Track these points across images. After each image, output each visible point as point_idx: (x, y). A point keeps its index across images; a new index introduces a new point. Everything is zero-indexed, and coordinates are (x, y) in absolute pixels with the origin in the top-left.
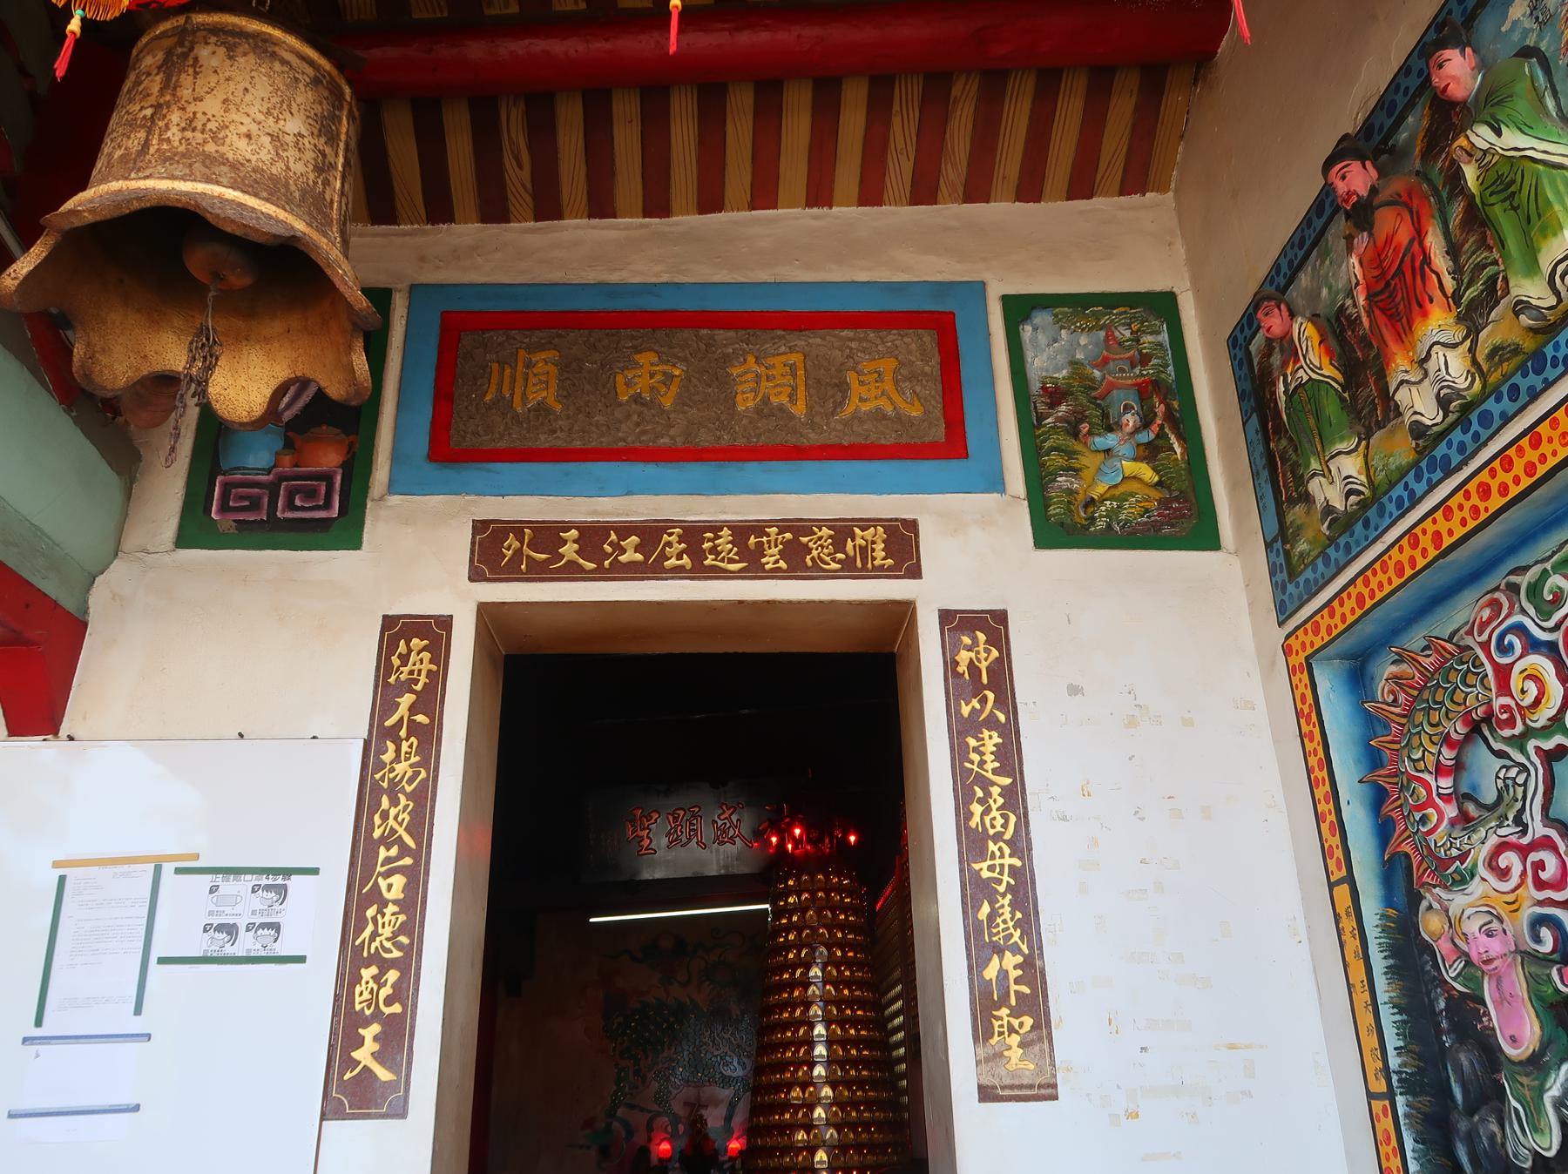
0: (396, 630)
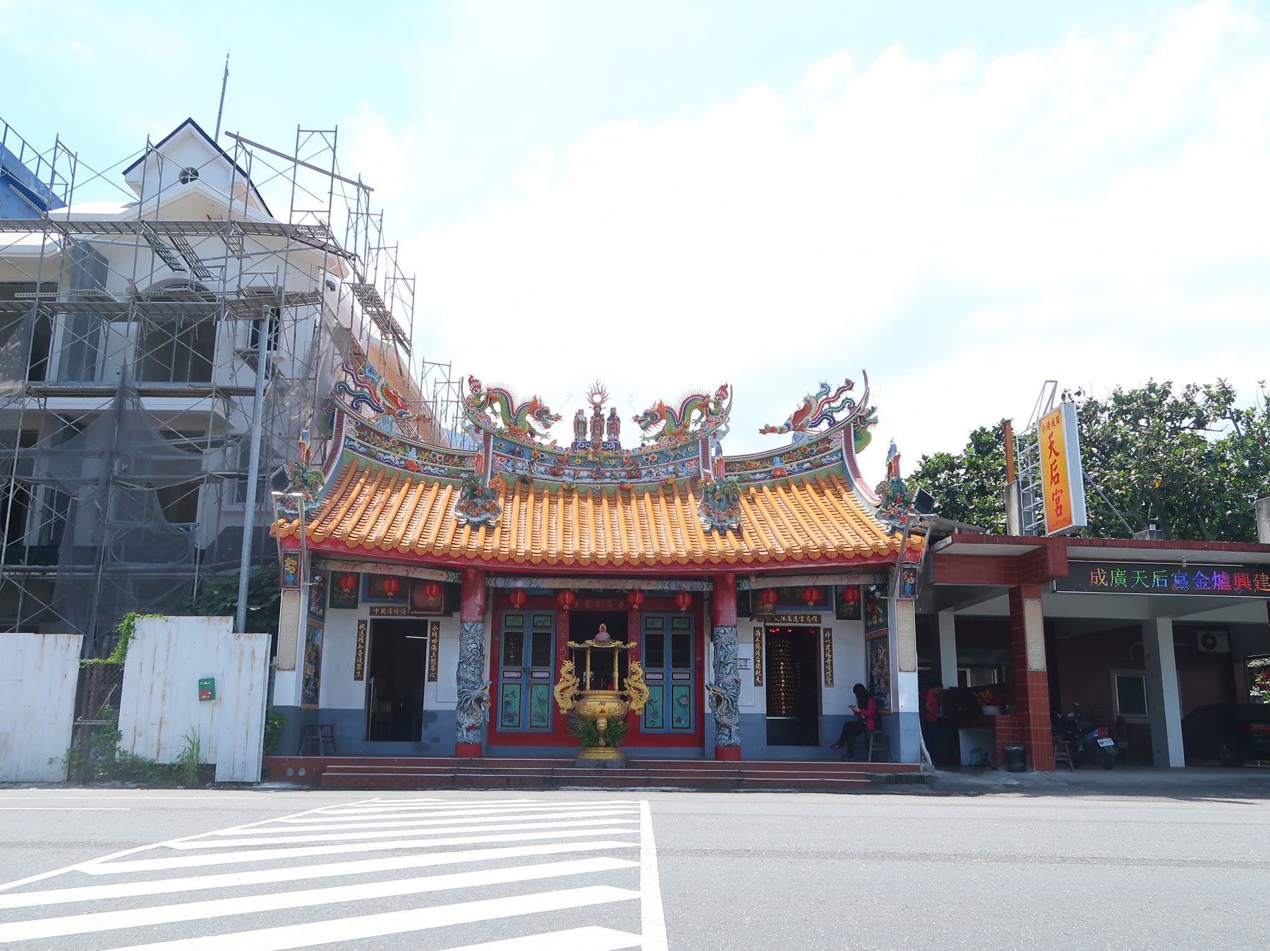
0: (360, 622)
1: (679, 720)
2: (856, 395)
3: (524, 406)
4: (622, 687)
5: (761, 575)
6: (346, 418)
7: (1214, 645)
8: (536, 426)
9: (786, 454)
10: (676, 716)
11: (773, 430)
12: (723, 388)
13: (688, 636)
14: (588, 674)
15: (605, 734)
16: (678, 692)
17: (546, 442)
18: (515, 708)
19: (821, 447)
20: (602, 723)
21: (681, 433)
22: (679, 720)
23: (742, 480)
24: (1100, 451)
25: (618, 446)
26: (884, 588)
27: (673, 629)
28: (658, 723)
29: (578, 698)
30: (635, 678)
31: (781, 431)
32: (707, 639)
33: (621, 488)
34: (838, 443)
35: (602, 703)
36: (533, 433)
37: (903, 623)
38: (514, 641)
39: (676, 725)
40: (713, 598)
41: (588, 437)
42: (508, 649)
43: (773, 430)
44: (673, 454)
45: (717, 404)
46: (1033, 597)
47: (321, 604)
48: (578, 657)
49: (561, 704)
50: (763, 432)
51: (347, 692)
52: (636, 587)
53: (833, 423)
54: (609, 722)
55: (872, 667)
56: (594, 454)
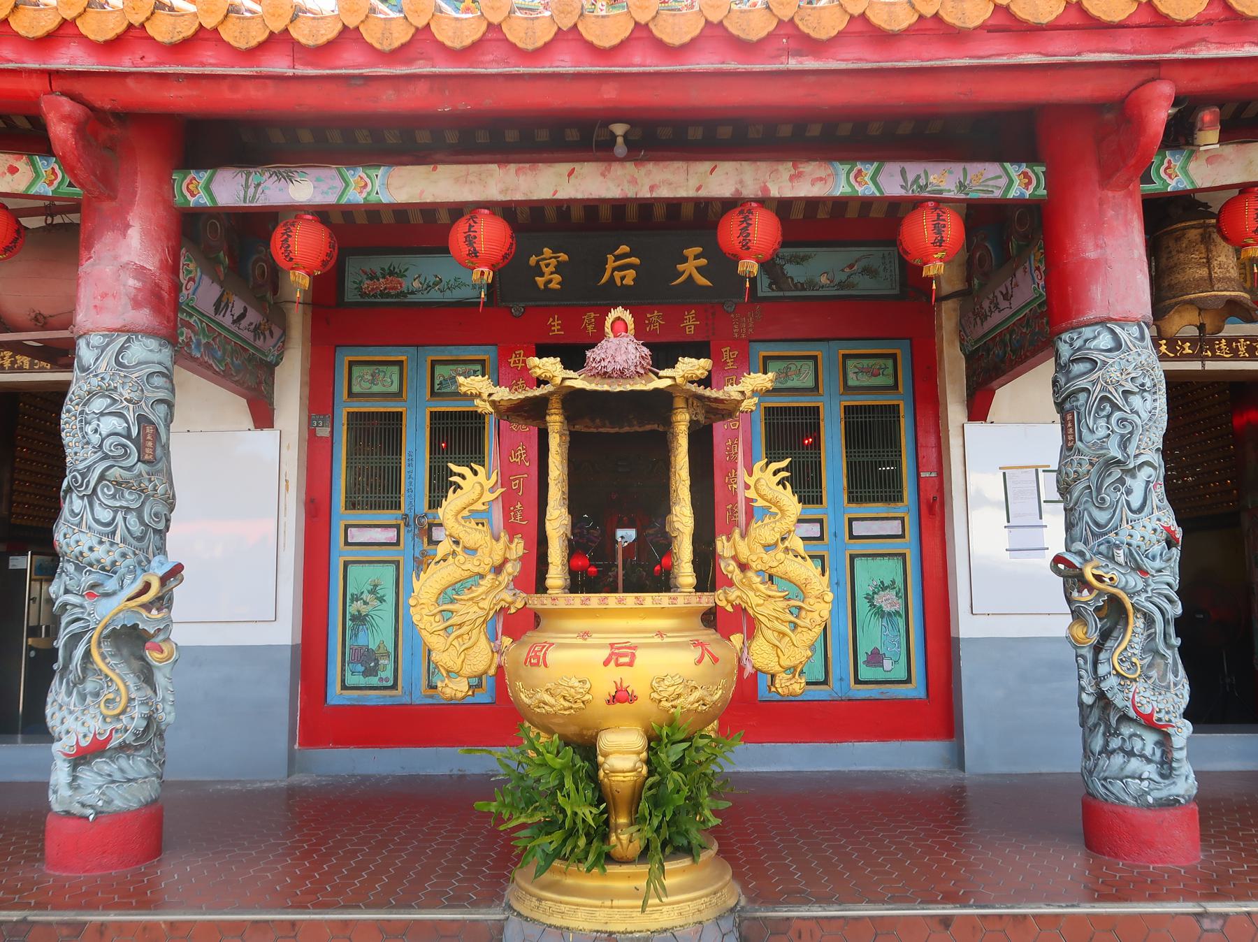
4: (708, 577)
10: (864, 649)
13: (894, 409)
15: (650, 795)
16: (869, 574)
18: (379, 636)
20: (622, 755)
22: (876, 658)
24: (1096, 262)
27: (848, 389)
30: (765, 531)
32: (955, 412)
35: (620, 655)
38: (377, 434)
39: (866, 673)
52: (751, 191)
54: (654, 741)
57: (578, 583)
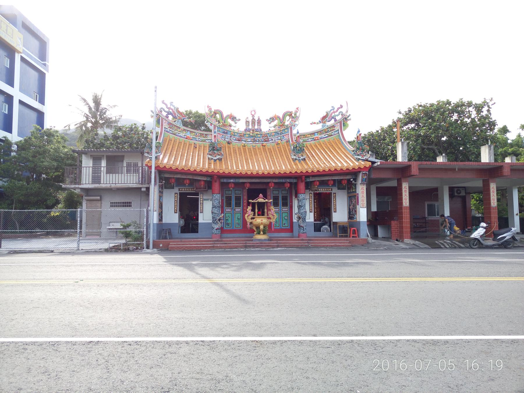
0: (175, 193)
1: (285, 224)
2: (343, 110)
3: (228, 116)
4: (268, 215)
5: (313, 176)
6: (164, 121)
7: (460, 193)
8: (232, 123)
9: (320, 132)
11: (315, 123)
12: (297, 108)
14: (257, 210)
17: (235, 129)
19: (331, 129)
20: (262, 227)
21: (283, 125)
22: (285, 224)
23: (304, 141)
25: (261, 130)
26: (355, 180)
28: (278, 225)
29: (252, 218)
31: (318, 123)
32: (294, 197)
33: (262, 145)
34: (337, 128)
36: (230, 126)
37: (361, 190)
38: (229, 199)
40: (296, 184)
41: (250, 127)
42: (227, 202)
43: (315, 123)
44: (279, 132)
45: (295, 114)
46: (405, 182)
47: (162, 188)
48: (253, 205)
49: (248, 220)
50: (311, 124)
51: (172, 217)
53: (336, 120)
54: (264, 227)
55: (350, 206)
56: (252, 133)
57: (258, 215)
